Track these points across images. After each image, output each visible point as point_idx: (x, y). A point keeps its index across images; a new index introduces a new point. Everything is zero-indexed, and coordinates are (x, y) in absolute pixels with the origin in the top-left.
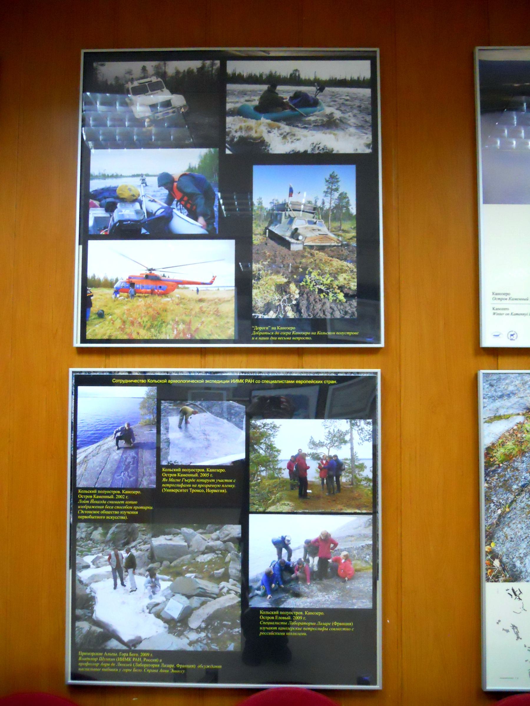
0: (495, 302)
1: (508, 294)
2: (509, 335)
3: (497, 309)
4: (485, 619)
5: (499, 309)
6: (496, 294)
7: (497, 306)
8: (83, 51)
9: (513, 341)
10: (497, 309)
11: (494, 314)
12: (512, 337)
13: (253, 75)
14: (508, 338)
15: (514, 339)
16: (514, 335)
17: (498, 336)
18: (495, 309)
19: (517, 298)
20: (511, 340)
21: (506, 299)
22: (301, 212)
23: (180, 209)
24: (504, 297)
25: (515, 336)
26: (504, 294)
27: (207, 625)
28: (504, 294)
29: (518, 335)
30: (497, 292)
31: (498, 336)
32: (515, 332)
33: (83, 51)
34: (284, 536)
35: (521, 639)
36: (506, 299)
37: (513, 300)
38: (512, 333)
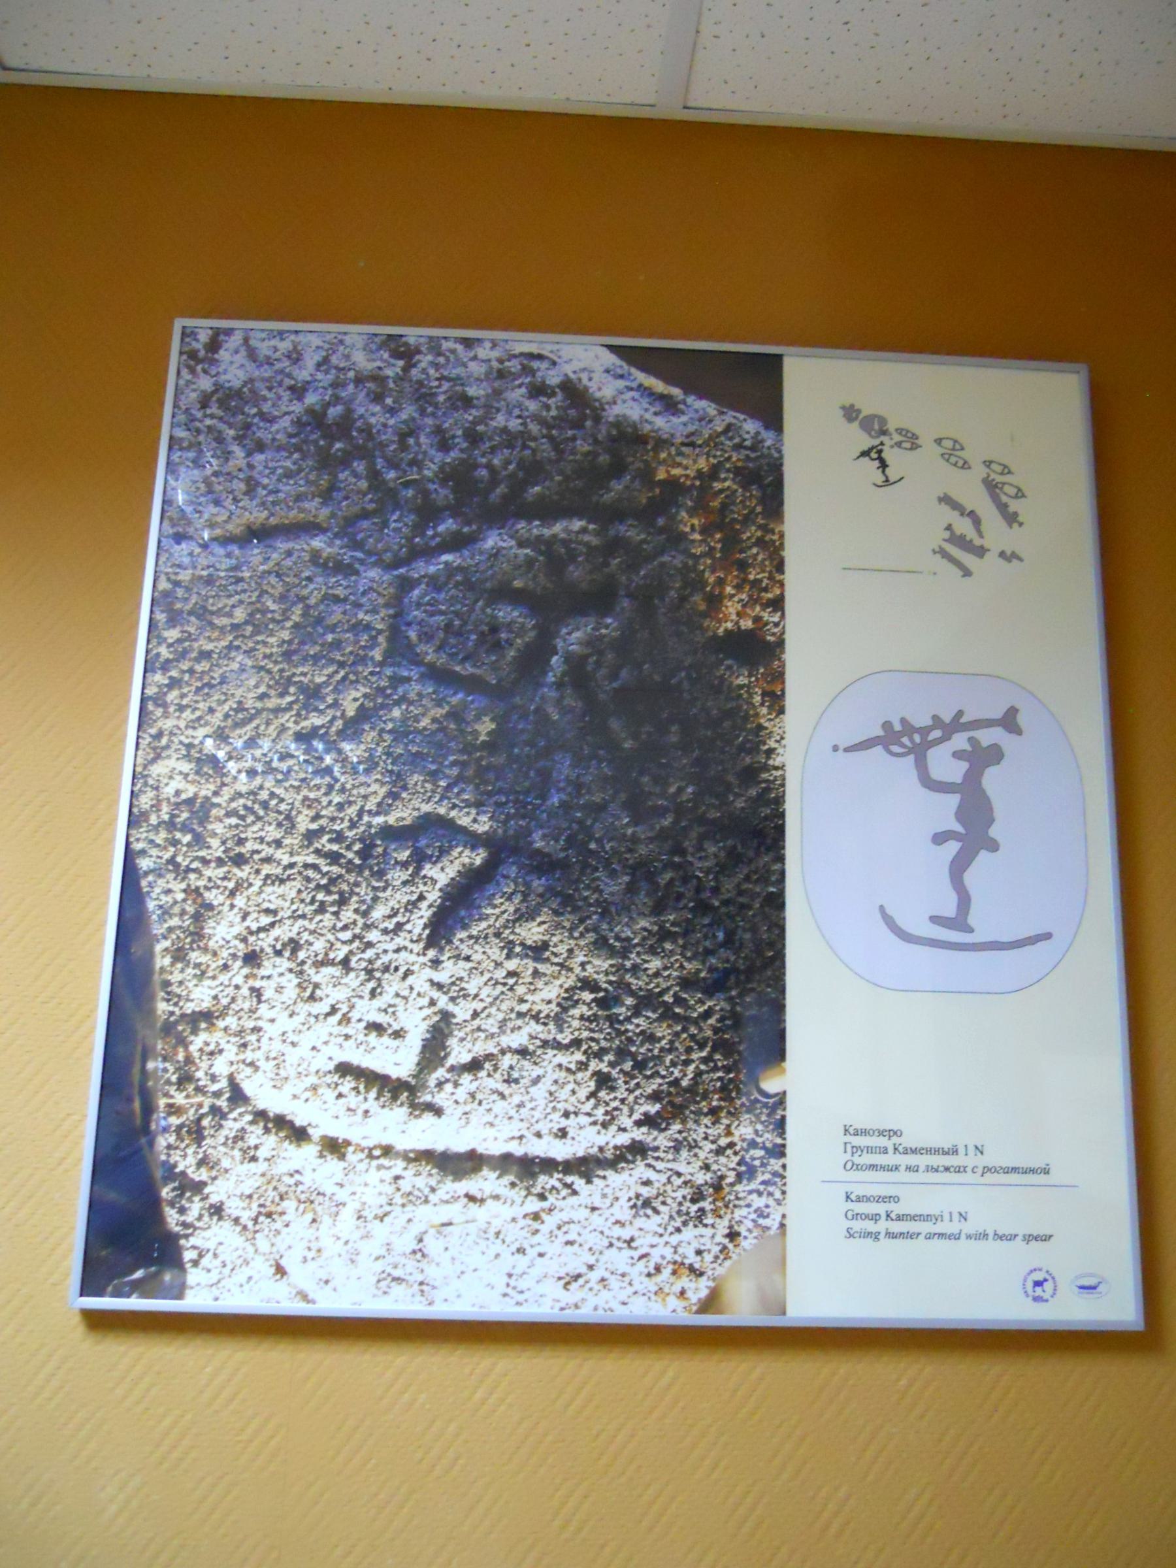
1: (895, 1133)
2: (1030, 1285)
3: (859, 1200)
4: (1128, 1145)
6: (856, 1133)
7: (859, 1190)
10: (900, 1218)
11: (851, 1235)
13: (968, 538)
14: (1027, 1296)
17: (1094, 1288)
18: (893, 1216)
19: (919, 1146)
20: (1037, 1299)
22: (310, 1150)
24: (882, 1142)
25: (1048, 1286)
26: (881, 1133)
28: (881, 1133)
30: (859, 1126)
31: (1094, 1288)
35: (1021, 524)
37: (906, 1152)
38: (1039, 1276)
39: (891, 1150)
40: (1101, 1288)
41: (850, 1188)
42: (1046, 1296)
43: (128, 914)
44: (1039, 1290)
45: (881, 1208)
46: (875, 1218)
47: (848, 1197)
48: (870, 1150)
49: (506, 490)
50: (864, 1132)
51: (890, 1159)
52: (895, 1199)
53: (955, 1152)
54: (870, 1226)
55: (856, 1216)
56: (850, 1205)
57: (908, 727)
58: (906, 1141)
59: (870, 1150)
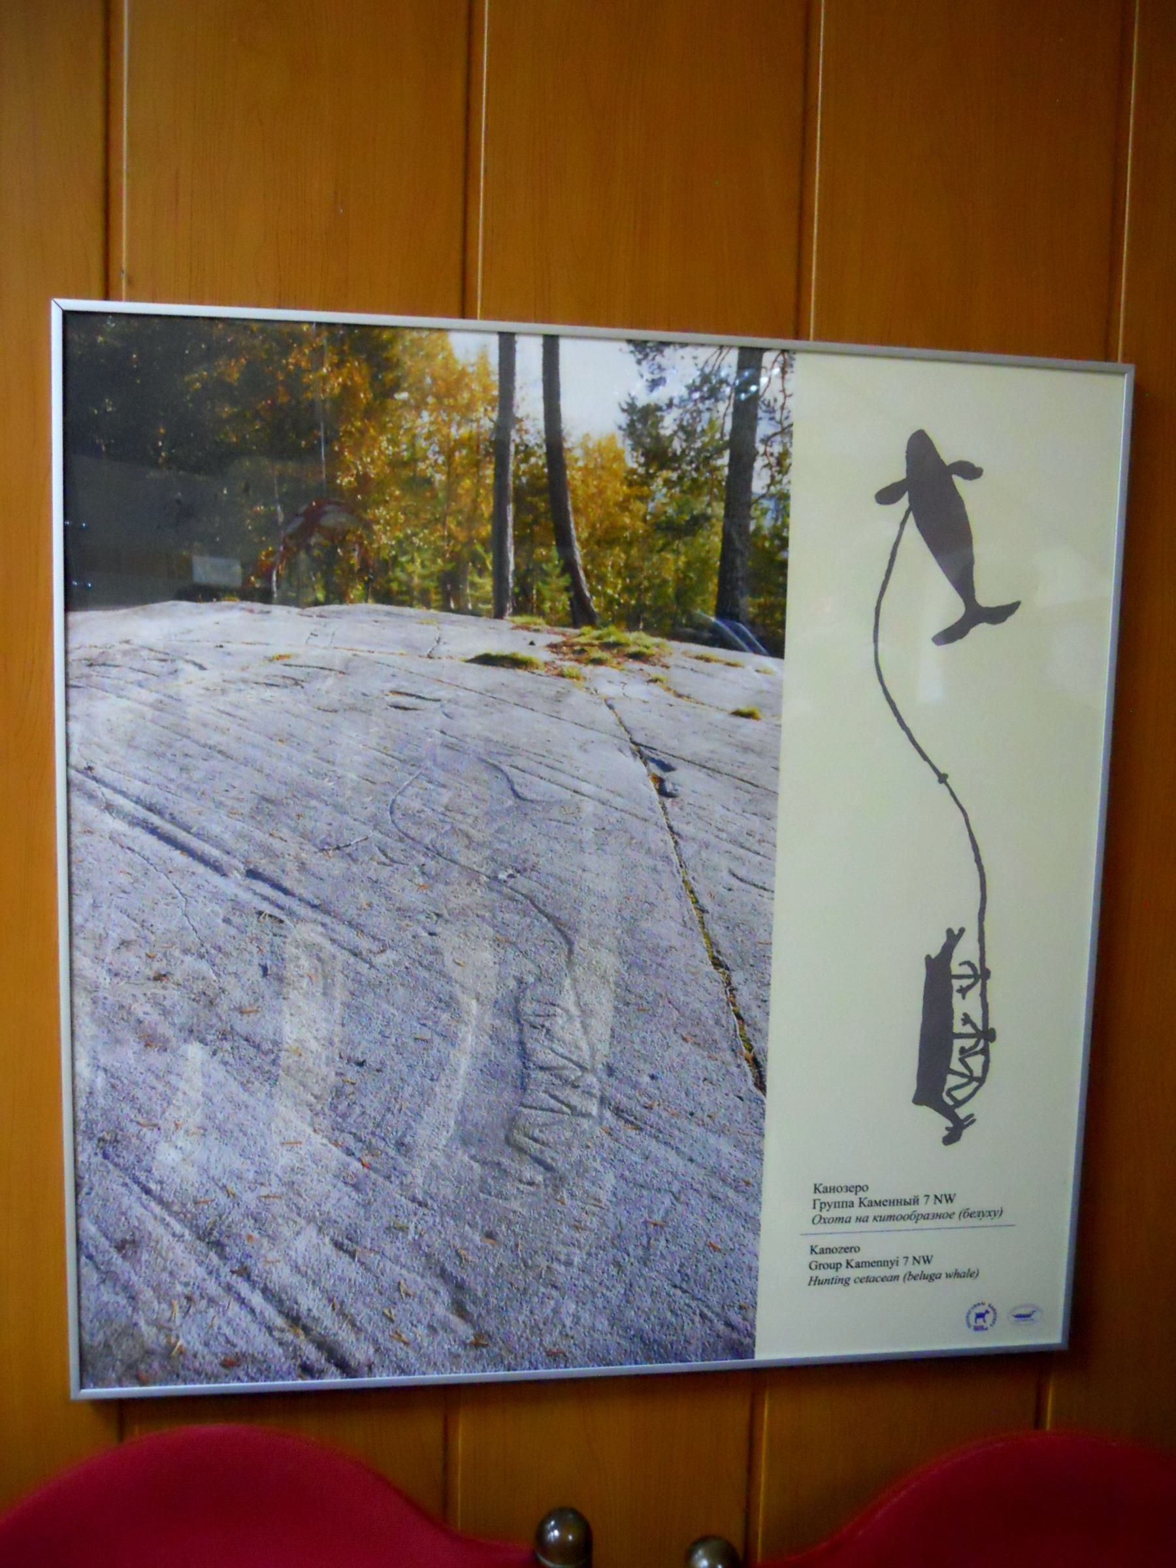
0: (822, 1228)
2: (972, 1317)
3: (822, 1251)
5: (831, 1251)
8: (58, 307)
9: (980, 1333)
10: (822, 1251)
12: (980, 1321)
14: (969, 1325)
15: (986, 1325)
16: (987, 1316)
20: (977, 1329)
21: (950, 1216)
23: (619, 663)
25: (989, 1317)
27: (344, 538)
29: (964, 1316)
32: (990, 1306)
33: (58, 307)
34: (624, 400)
36: (950, 1216)
38: (981, 1310)
48: (837, 1205)
50: (834, 1189)
53: (916, 1201)
58: (871, 1195)
59: (837, 1205)
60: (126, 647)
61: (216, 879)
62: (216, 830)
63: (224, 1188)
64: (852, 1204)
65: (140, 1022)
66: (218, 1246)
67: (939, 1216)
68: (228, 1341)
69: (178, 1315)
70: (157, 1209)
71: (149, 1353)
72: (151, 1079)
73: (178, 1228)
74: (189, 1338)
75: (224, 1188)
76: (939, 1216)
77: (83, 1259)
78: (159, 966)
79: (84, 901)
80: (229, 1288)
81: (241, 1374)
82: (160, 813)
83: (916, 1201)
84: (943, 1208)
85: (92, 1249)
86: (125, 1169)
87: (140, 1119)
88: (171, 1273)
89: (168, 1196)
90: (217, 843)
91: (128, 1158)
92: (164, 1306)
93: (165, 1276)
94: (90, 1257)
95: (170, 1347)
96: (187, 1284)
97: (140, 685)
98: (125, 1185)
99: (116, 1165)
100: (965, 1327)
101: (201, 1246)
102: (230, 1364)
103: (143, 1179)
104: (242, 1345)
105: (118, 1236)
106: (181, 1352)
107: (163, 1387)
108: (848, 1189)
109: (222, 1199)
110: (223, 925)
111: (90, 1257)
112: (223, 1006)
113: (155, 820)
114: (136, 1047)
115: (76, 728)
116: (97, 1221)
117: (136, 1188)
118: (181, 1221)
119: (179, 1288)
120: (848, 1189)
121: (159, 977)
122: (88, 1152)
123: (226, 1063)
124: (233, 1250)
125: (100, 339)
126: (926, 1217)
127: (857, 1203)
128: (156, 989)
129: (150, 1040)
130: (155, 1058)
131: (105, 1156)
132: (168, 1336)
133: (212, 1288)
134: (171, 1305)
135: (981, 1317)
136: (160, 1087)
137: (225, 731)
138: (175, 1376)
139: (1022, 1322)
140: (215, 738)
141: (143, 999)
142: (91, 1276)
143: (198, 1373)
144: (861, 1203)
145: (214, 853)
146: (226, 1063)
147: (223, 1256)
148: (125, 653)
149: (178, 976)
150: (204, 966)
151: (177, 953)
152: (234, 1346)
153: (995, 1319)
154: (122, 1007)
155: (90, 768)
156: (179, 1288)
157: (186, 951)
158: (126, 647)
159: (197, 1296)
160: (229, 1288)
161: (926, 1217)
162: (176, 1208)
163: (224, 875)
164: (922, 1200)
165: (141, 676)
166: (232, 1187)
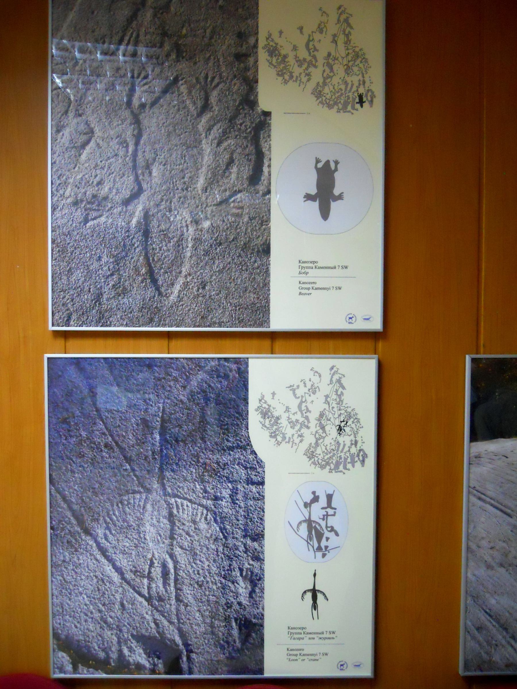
2: (348, 318)
7: (291, 647)
9: (342, 671)
10: (304, 655)
11: (300, 294)
14: (338, 668)
15: (344, 668)
24: (300, 631)
25: (345, 666)
31: (359, 666)
38: (351, 316)
39: (314, 268)
40: (361, 666)
41: (288, 646)
42: (353, 322)
43: (92, 362)
44: (350, 320)
45: (310, 286)
46: (296, 655)
47: (300, 282)
48: (296, 633)
49: (103, 658)
50: (294, 628)
51: (302, 636)
52: (303, 650)
53: (323, 633)
54: (306, 291)
55: (302, 288)
56: (300, 285)
57: (346, 70)
58: (307, 631)
59: (296, 633)
60: (486, 452)
61: (509, 519)
62: (510, 504)
63: (508, 611)
64: (301, 634)
65: (486, 561)
66: (506, 629)
67: (329, 638)
68: (507, 659)
69: (493, 650)
70: (489, 618)
71: (485, 662)
72: (488, 578)
73: (494, 623)
74: (496, 658)
75: (508, 611)
76: (329, 638)
77: (467, 633)
78: (492, 545)
79: (471, 526)
80: (509, 643)
81: (511, 669)
82: (494, 500)
83: (323, 633)
84: (332, 636)
85: (469, 630)
86: (479, 606)
87: (484, 590)
88: (492, 638)
89: (492, 614)
90: (509, 508)
91: (480, 602)
92: (489, 647)
93: (490, 638)
94: (468, 632)
95: (490, 660)
96: (496, 641)
97: (490, 463)
98: (480, 610)
99: (477, 604)
100: (336, 667)
101: (500, 629)
102: (508, 666)
103: (485, 608)
104: (511, 660)
105: (477, 626)
106: (494, 662)
107: (247, 676)
108: (300, 628)
109: (507, 614)
110: (511, 532)
111: (468, 632)
112: (510, 556)
113: (493, 502)
114: (485, 569)
115: (472, 476)
116: (471, 621)
117: (483, 611)
118: (495, 621)
119: (494, 642)
120: (300, 628)
121: (492, 548)
122: (470, 600)
123: (510, 573)
124: (511, 631)
125: (481, 365)
126: (325, 638)
127: (303, 633)
128: (491, 552)
129: (489, 567)
130: (490, 572)
131: (474, 601)
132: (490, 657)
133: (504, 642)
134: (491, 647)
135: (342, 666)
136: (491, 581)
137: (512, 476)
138: (490, 669)
139: (357, 668)
140: (510, 478)
141: (487, 555)
142: (469, 638)
143: (498, 669)
144: (304, 633)
145: (509, 511)
146: (510, 573)
147: (507, 632)
148: (486, 454)
149: (497, 548)
150: (504, 545)
151: (497, 541)
152: (509, 660)
153: (347, 667)
154: (481, 557)
155: (475, 487)
156: (494, 642)
157: (500, 540)
158: (486, 452)
159: (499, 645)
160: (509, 643)
161: (325, 638)
162: (494, 617)
163: (511, 517)
164: (325, 633)
165: (490, 460)
166: (511, 611)
